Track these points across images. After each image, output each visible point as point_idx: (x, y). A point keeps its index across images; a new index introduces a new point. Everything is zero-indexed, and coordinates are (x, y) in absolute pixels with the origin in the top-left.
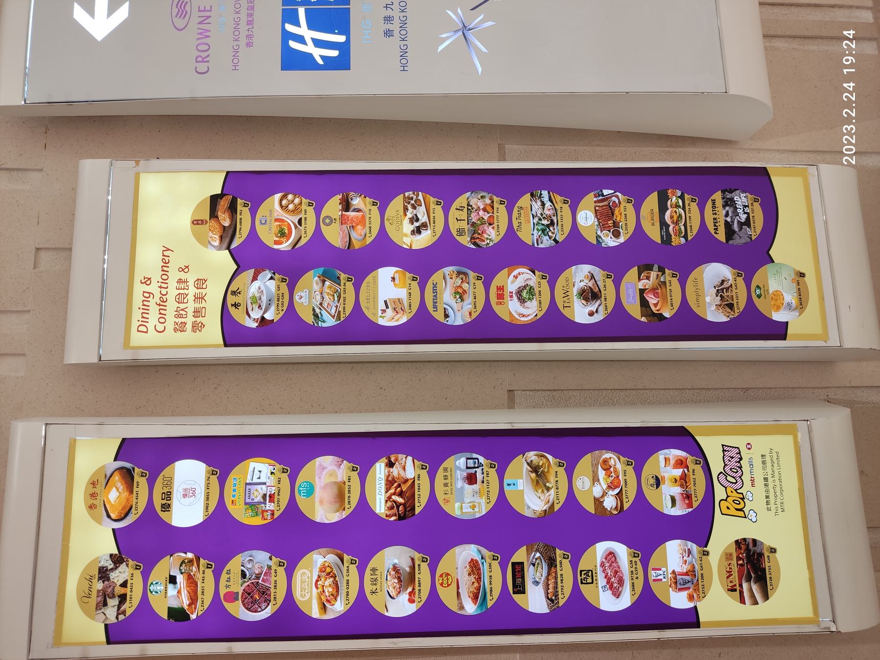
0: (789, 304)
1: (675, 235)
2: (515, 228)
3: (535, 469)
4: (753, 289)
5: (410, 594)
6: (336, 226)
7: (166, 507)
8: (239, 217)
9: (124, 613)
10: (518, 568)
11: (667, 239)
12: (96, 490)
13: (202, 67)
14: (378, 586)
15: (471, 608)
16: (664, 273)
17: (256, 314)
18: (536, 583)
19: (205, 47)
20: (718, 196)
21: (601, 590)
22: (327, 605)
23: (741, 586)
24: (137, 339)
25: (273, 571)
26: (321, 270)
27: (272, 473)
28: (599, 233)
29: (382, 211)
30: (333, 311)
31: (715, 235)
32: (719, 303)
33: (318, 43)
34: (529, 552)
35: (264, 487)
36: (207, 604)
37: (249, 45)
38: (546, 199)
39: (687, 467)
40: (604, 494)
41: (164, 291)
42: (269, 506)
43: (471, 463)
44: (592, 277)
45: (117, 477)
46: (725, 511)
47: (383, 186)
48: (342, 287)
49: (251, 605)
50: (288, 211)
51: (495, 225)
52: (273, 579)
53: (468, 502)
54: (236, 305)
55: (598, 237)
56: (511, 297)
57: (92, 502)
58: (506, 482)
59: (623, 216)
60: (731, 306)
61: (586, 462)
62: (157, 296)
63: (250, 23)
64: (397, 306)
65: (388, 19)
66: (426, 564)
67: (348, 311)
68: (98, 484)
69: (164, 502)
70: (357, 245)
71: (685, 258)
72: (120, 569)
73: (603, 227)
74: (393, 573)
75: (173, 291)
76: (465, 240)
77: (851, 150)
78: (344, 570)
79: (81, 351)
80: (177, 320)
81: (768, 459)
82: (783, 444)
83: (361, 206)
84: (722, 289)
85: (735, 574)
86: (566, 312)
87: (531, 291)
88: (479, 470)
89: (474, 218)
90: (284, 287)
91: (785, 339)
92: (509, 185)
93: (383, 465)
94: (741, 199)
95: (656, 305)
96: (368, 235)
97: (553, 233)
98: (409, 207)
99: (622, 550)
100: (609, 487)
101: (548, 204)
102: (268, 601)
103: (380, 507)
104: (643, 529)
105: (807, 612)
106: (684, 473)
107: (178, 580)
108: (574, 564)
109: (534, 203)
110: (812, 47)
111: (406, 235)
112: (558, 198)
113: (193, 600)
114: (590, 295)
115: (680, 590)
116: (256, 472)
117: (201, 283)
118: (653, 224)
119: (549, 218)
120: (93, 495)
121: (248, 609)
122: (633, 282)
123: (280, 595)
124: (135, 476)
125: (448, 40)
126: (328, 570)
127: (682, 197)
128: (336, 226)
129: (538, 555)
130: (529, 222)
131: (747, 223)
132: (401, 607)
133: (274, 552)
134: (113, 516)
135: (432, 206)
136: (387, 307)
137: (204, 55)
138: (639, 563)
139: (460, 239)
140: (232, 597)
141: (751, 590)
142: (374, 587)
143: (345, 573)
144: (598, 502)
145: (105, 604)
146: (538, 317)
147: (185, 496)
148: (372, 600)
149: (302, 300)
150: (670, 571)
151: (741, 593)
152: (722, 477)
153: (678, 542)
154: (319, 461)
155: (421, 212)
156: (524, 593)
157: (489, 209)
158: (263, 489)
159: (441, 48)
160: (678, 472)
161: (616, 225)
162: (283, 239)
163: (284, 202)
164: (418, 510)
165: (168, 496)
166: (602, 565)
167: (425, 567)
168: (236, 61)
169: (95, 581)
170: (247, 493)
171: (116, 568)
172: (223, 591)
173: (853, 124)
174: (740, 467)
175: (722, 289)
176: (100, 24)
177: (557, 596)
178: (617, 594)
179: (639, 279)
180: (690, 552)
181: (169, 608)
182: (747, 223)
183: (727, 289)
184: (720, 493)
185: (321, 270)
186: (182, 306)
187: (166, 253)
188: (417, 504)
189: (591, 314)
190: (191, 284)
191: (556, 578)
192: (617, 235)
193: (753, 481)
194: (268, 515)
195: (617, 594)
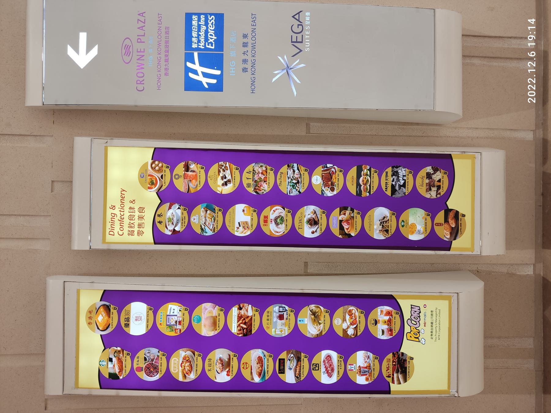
0: (419, 231)
3: (314, 313)
4: (400, 222)
5: (227, 372)
6: (181, 180)
7: (127, 325)
10: (282, 361)
11: (359, 193)
12: (92, 315)
13: (140, 87)
14: (212, 367)
15: (257, 379)
16: (353, 212)
17: (171, 227)
18: (290, 369)
19: (142, 75)
20: (389, 170)
21: (322, 373)
22: (187, 375)
23: (393, 375)
24: (109, 238)
25: (160, 358)
26: (205, 205)
28: (323, 188)
29: (207, 172)
30: (211, 227)
32: (381, 229)
33: (205, 75)
34: (288, 354)
35: (176, 317)
36: (128, 372)
37: (166, 74)
38: (296, 168)
40: (348, 327)
41: (122, 213)
42: (179, 327)
43: (281, 309)
44: (315, 212)
45: (102, 309)
47: (207, 158)
48: (216, 214)
49: (149, 374)
50: (156, 171)
51: (267, 182)
52: (160, 362)
54: (160, 222)
56: (271, 222)
57: (89, 321)
58: (298, 319)
59: (337, 179)
60: (387, 231)
61: (340, 311)
62: (119, 216)
63: (167, 61)
64: (245, 225)
65: (245, 61)
66: (236, 358)
67: (219, 228)
68: (92, 313)
69: (126, 322)
70: (192, 191)
71: (362, 204)
73: (325, 185)
74: (219, 361)
75: (127, 214)
76: (251, 190)
77: (533, 94)
78: (195, 359)
79: (80, 242)
80: (129, 229)
81: (434, 313)
83: (195, 169)
84: (384, 222)
85: (391, 369)
86: (299, 231)
87: (282, 219)
88: (285, 313)
89: (256, 178)
90: (185, 213)
91: (449, 250)
92: (276, 160)
93: (236, 309)
94: (402, 172)
95: (347, 229)
96: (198, 185)
99: (334, 355)
100: (351, 324)
101: (297, 171)
102: (157, 372)
103: (234, 329)
105: (444, 387)
106: (390, 319)
108: (310, 361)
109: (289, 170)
110: (495, 63)
111: (219, 186)
112: (302, 168)
113: (121, 370)
114: (313, 222)
115: (362, 375)
116: (172, 309)
117: (141, 210)
119: (297, 179)
120: (90, 318)
121: (148, 375)
122: (336, 216)
123: (163, 369)
125: (279, 74)
126: (187, 359)
127: (370, 170)
128: (181, 180)
129: (292, 355)
130: (286, 181)
131: (404, 185)
132: (223, 378)
133: (160, 349)
134: (100, 328)
135: (234, 170)
136: (240, 226)
137: (141, 79)
138: (342, 361)
139: (248, 189)
140: (140, 369)
141: (398, 377)
142: (210, 368)
143: (195, 361)
147: (136, 320)
148: (210, 374)
150: (358, 366)
151: (393, 378)
152: (409, 321)
153: (363, 352)
154: (204, 305)
156: (284, 373)
157: (264, 173)
159: (274, 80)
160: (387, 318)
161: (333, 184)
162: (153, 186)
163: (153, 165)
164: (253, 332)
165: (128, 319)
166: (324, 361)
167: (235, 359)
168: (159, 84)
170: (167, 320)
172: (135, 366)
174: (419, 317)
175: (383, 222)
176: (82, 56)
178: (330, 376)
179: (340, 215)
180: (369, 357)
182: (404, 185)
183: (386, 222)
184: (407, 329)
185: (205, 205)
186: (132, 222)
188: (253, 329)
189: (313, 233)
190: (136, 210)
191: (300, 367)
192: (332, 189)
193: (425, 324)
195: (330, 376)
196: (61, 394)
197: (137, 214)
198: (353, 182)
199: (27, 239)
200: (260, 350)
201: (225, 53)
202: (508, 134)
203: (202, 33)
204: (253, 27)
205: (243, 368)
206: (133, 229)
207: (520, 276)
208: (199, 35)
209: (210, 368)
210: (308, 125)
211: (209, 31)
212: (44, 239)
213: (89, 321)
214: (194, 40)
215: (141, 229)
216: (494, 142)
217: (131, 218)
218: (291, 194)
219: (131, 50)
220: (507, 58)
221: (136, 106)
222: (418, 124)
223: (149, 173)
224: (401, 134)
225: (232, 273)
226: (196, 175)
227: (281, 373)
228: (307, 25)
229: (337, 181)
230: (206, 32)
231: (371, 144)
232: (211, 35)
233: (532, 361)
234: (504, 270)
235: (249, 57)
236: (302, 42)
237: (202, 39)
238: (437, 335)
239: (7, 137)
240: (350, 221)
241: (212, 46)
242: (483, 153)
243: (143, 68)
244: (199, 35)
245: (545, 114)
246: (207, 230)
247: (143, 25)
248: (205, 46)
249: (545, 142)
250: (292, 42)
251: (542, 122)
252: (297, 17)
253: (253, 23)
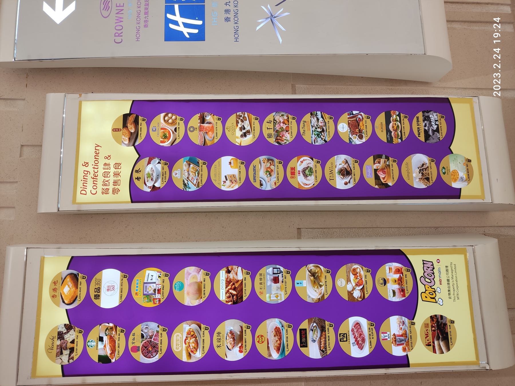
0: (462, 178)
1: (395, 137)
2: (302, 133)
3: (313, 274)
4: (440, 169)
5: (240, 347)
6: (197, 132)
7: (97, 297)
8: (140, 127)
9: (72, 358)
10: (303, 332)
11: (390, 140)
12: (56, 287)
13: (118, 39)
14: (221, 343)
15: (275, 356)
16: (388, 160)
17: (150, 184)
18: (314, 341)
19: (120, 28)
20: (420, 115)
21: (351, 345)
22: (191, 354)
23: (434, 342)
24: (80, 198)
25: (160, 334)
26: (188, 158)
27: (159, 277)
28: (351, 136)
29: (224, 124)
30: (195, 182)
31: (419, 138)
32: (420, 177)
33: (186, 25)
34: (309, 323)
35: (154, 285)
36: (121, 354)
37: (146, 26)
38: (319, 116)
39: (402, 273)
40: (354, 289)
41: (96, 170)
42: (158, 296)
43: (275, 271)
44: (347, 162)
45: (68, 279)
46: (424, 299)
47: (224, 109)
48: (200, 168)
49: (147, 354)
50: (169, 124)
51: (290, 132)
52: (160, 339)
53: (274, 294)
54: (138, 179)
55: (350, 139)
56: (299, 173)
57: (54, 293)
58: (296, 282)
59: (365, 126)
60: (428, 179)
61: (343, 270)
62: (92, 173)
63: (146, 13)
64: (232, 179)
65: (227, 11)
66: (249, 330)
67: (204, 182)
68: (57, 283)
69: (96, 293)
70: (209, 143)
71: (401, 151)
72: (70, 333)
73: (353, 133)
74: (230, 335)
75: (101, 170)
76: (272, 141)
77: (498, 88)
78: (202, 333)
79: (47, 205)
80: (103, 187)
81: (449, 268)
82: (458, 260)
83: (212, 120)
84: (423, 169)
85: (430, 336)
86: (331, 182)
87: (311, 170)
88: (280, 275)
89: (277, 128)
90: (166, 168)
91: (459, 198)
92: (298, 108)
93: (224, 272)
94: (434, 116)
95: (384, 178)
96: (215, 137)
97: (324, 136)
98: (240, 121)
99: (364, 322)
100: (357, 285)
101: (321, 119)
102: (157, 352)
103: (222, 296)
104: (376, 309)
106: (400, 277)
107: (104, 339)
108: (336, 330)
109: (312, 119)
111: (238, 138)
112: (327, 116)
113: (113, 351)
114: (345, 172)
115: (398, 345)
116: (150, 276)
117: (117, 165)
118: (382, 131)
119: (321, 127)
120: (55, 290)
121: (145, 356)
122: (370, 165)
123: (164, 348)
124: (79, 278)
125: (262, 23)
126: (192, 333)
127: (399, 115)
128: (197, 132)
129: (315, 324)
130: (309, 130)
131: (437, 130)
132: (235, 355)
133: (160, 323)
134: (66, 302)
135: (253, 120)
136: (227, 180)
137: (119, 32)
138: (374, 329)
139: (269, 140)
140: (136, 349)
141: (439, 345)
142: (219, 344)
143: (202, 335)
144: (350, 294)
145: (62, 353)
146: (315, 185)
147: (108, 290)
148: (218, 351)
149: (177, 175)
150: (392, 334)
151: (434, 347)
152: (422, 279)
153: (397, 317)
154: (186, 269)
155: (246, 124)
156: (307, 347)
157: (286, 122)
158: (154, 286)
159: (258, 28)
160: (397, 276)
161: (360, 131)
162: (166, 140)
163: (166, 118)
164: (244, 298)
165: (98, 290)
166: (353, 330)
167: (249, 331)
168: (138, 36)
169: (56, 340)
170: (145, 288)
171: (68, 332)
172: (130, 346)
173: (499, 72)
174: (433, 273)
175: (423, 169)
177: (326, 349)
178: (361, 348)
179: (374, 163)
180: (404, 323)
181: (99, 356)
182: (437, 130)
183: (426, 169)
184: (421, 288)
185: (188, 158)
186: (107, 179)
187: (97, 148)
188: (244, 295)
189: (346, 184)
190: (112, 166)
191: (325, 338)
192: (361, 137)
193: (440, 281)
194: (157, 301)
195: (361, 348)
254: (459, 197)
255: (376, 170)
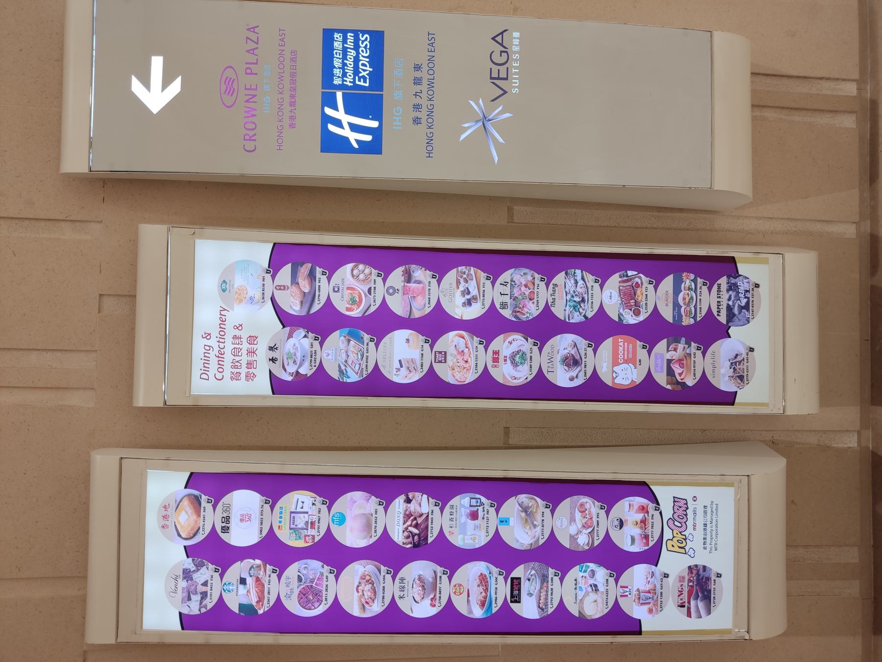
1: (686, 316)
3: (525, 510)
5: (432, 599)
7: (225, 530)
8: (317, 284)
9: (205, 607)
11: (678, 316)
12: (168, 513)
13: (250, 145)
14: (405, 592)
15: (478, 613)
16: (690, 346)
17: (292, 369)
18: (530, 595)
20: (723, 281)
22: (366, 605)
23: (689, 602)
25: (325, 578)
27: (313, 504)
28: (621, 311)
31: (718, 318)
32: (732, 374)
33: (354, 128)
34: (525, 570)
35: (306, 515)
37: (292, 126)
38: (579, 278)
39: (648, 512)
40: (579, 532)
41: (222, 345)
42: (311, 532)
43: (474, 502)
44: (575, 345)
45: (186, 503)
46: (670, 548)
48: (365, 347)
52: (325, 583)
53: (468, 534)
55: (620, 315)
56: (505, 360)
62: (216, 349)
63: (292, 104)
69: (224, 525)
72: (201, 571)
74: (418, 582)
75: (229, 347)
79: (146, 395)
80: (233, 370)
82: (724, 499)
85: (685, 594)
86: (549, 376)
88: (480, 509)
95: (680, 374)
96: (427, 305)
98: (462, 280)
101: (581, 282)
102: (320, 601)
104: (614, 559)
107: (248, 582)
109: (568, 281)
110: (797, 117)
113: (260, 600)
114: (572, 362)
116: (300, 503)
117: (252, 339)
118: (667, 305)
125: (470, 129)
126: (368, 578)
127: (695, 281)
128: (398, 296)
129: (533, 572)
132: (423, 610)
133: (326, 562)
134: (183, 536)
136: (401, 366)
137: (251, 133)
141: (697, 607)
142: (402, 593)
145: (189, 599)
146: (529, 380)
147: (242, 520)
149: (330, 357)
150: (635, 589)
151: (689, 609)
152: (671, 522)
153: (645, 565)
154: (349, 495)
159: (463, 137)
160: (640, 516)
161: (637, 304)
162: (355, 307)
163: (355, 272)
164: (430, 540)
165: (227, 520)
169: (180, 580)
170: (292, 520)
171: (198, 570)
174: (686, 515)
175: (736, 363)
176: (156, 94)
177: (546, 606)
179: (668, 351)
181: (240, 604)
183: (740, 362)
184: (668, 534)
185: (346, 330)
186: (237, 358)
187: (223, 313)
188: (430, 535)
189: (572, 379)
190: (244, 340)
191: (547, 591)
192: (637, 313)
194: (309, 539)
196: (113, 642)
197: (245, 346)
198: (667, 300)
199: (58, 388)
200: (482, 563)
201: (385, 93)
202: (818, 227)
203: (350, 62)
204: (431, 54)
205: (455, 593)
206: (238, 370)
207: (838, 449)
208: (344, 65)
209: (402, 593)
210: (510, 210)
211: (361, 58)
212: (85, 389)
213: (163, 522)
214: (337, 72)
215: (251, 371)
216: (800, 239)
217: (236, 352)
218: (572, 321)
219: (235, 86)
220: (815, 110)
221: (243, 176)
222: (681, 210)
223: (347, 284)
224: (655, 226)
225: (390, 445)
226: (423, 288)
227: (516, 602)
228: (515, 52)
229: (644, 299)
230: (356, 60)
231: (609, 239)
232: (363, 65)
233: (857, 583)
234: (813, 440)
235: (424, 101)
236: (506, 79)
237: (350, 73)
238: (713, 543)
239: (27, 222)
240: (685, 362)
241: (365, 82)
242: (787, 255)
243: (253, 115)
244: (344, 65)
245: (874, 197)
246: (350, 372)
247: (255, 46)
248: (354, 82)
249: (874, 239)
250: (491, 78)
251: (870, 209)
252: (499, 39)
253: (430, 47)
254: (732, 403)
255: (669, 361)
